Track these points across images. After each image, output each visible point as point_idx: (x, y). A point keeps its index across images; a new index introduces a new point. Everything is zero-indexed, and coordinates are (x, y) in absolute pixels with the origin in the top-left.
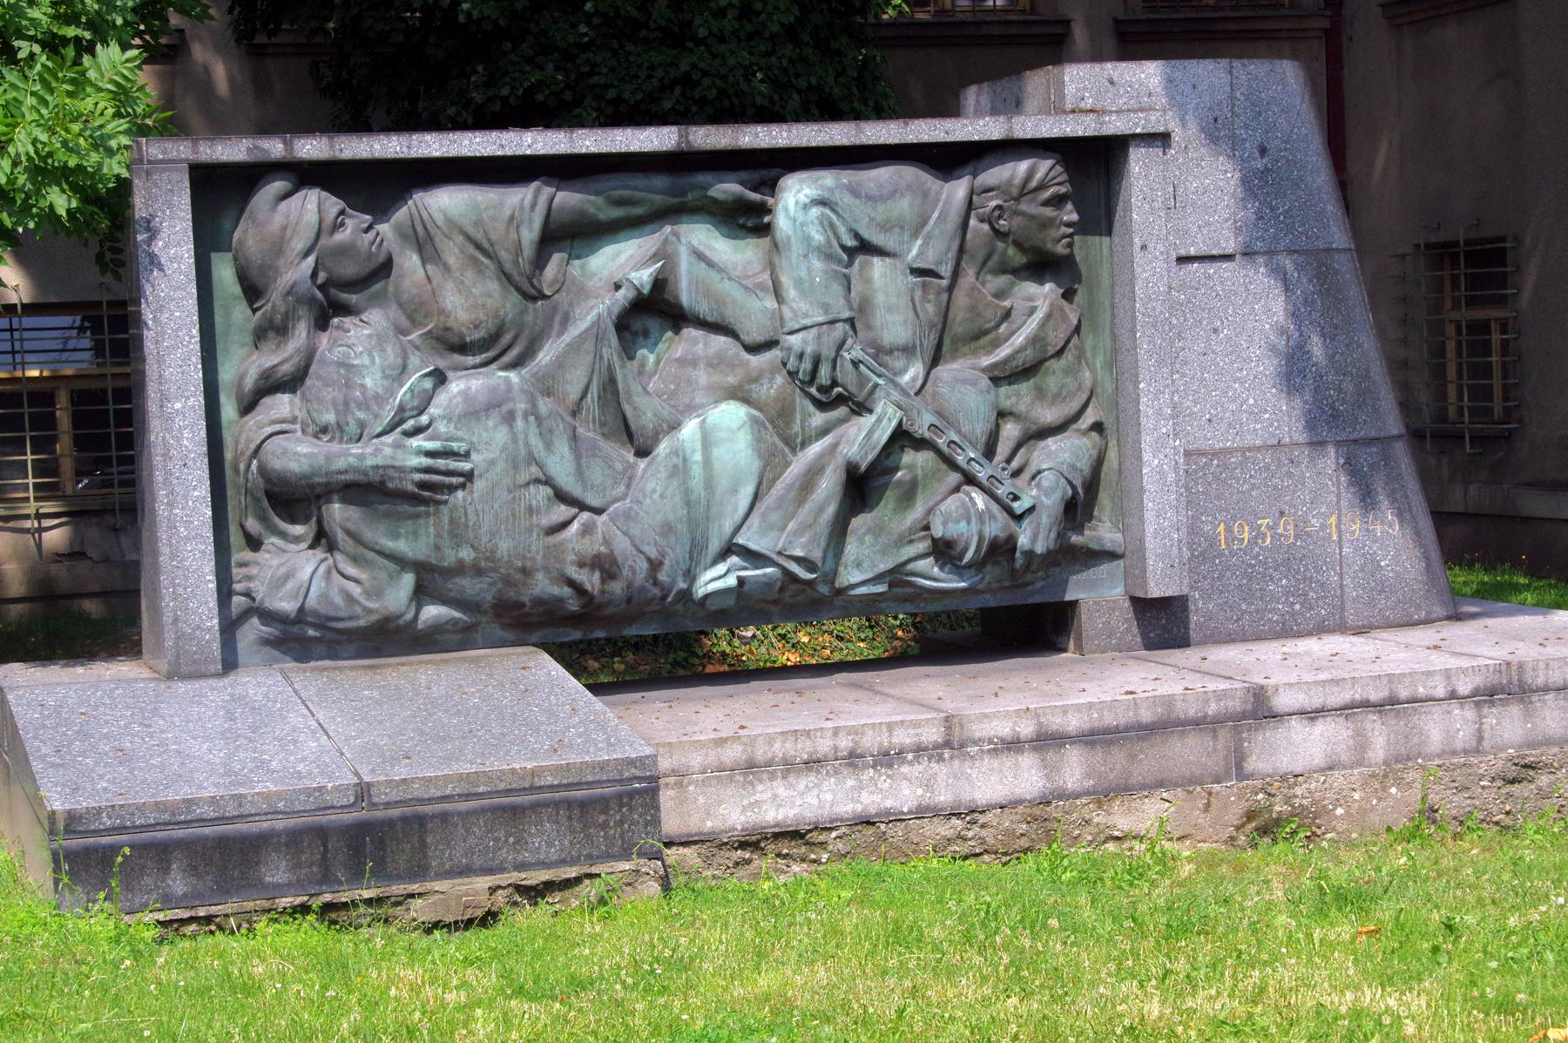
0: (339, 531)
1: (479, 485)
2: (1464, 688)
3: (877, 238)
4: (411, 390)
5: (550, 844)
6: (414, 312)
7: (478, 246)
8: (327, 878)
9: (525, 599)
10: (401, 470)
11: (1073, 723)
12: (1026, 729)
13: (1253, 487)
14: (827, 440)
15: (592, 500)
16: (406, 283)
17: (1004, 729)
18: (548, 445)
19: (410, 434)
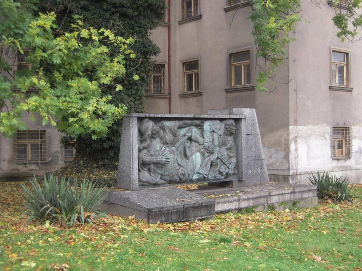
0: (152, 170)
1: (170, 163)
2: (289, 192)
3: (215, 130)
6: (161, 139)
7: (170, 129)
9: (173, 180)
10: (162, 161)
14: (209, 158)
15: (183, 166)
16: (161, 135)
18: (178, 158)
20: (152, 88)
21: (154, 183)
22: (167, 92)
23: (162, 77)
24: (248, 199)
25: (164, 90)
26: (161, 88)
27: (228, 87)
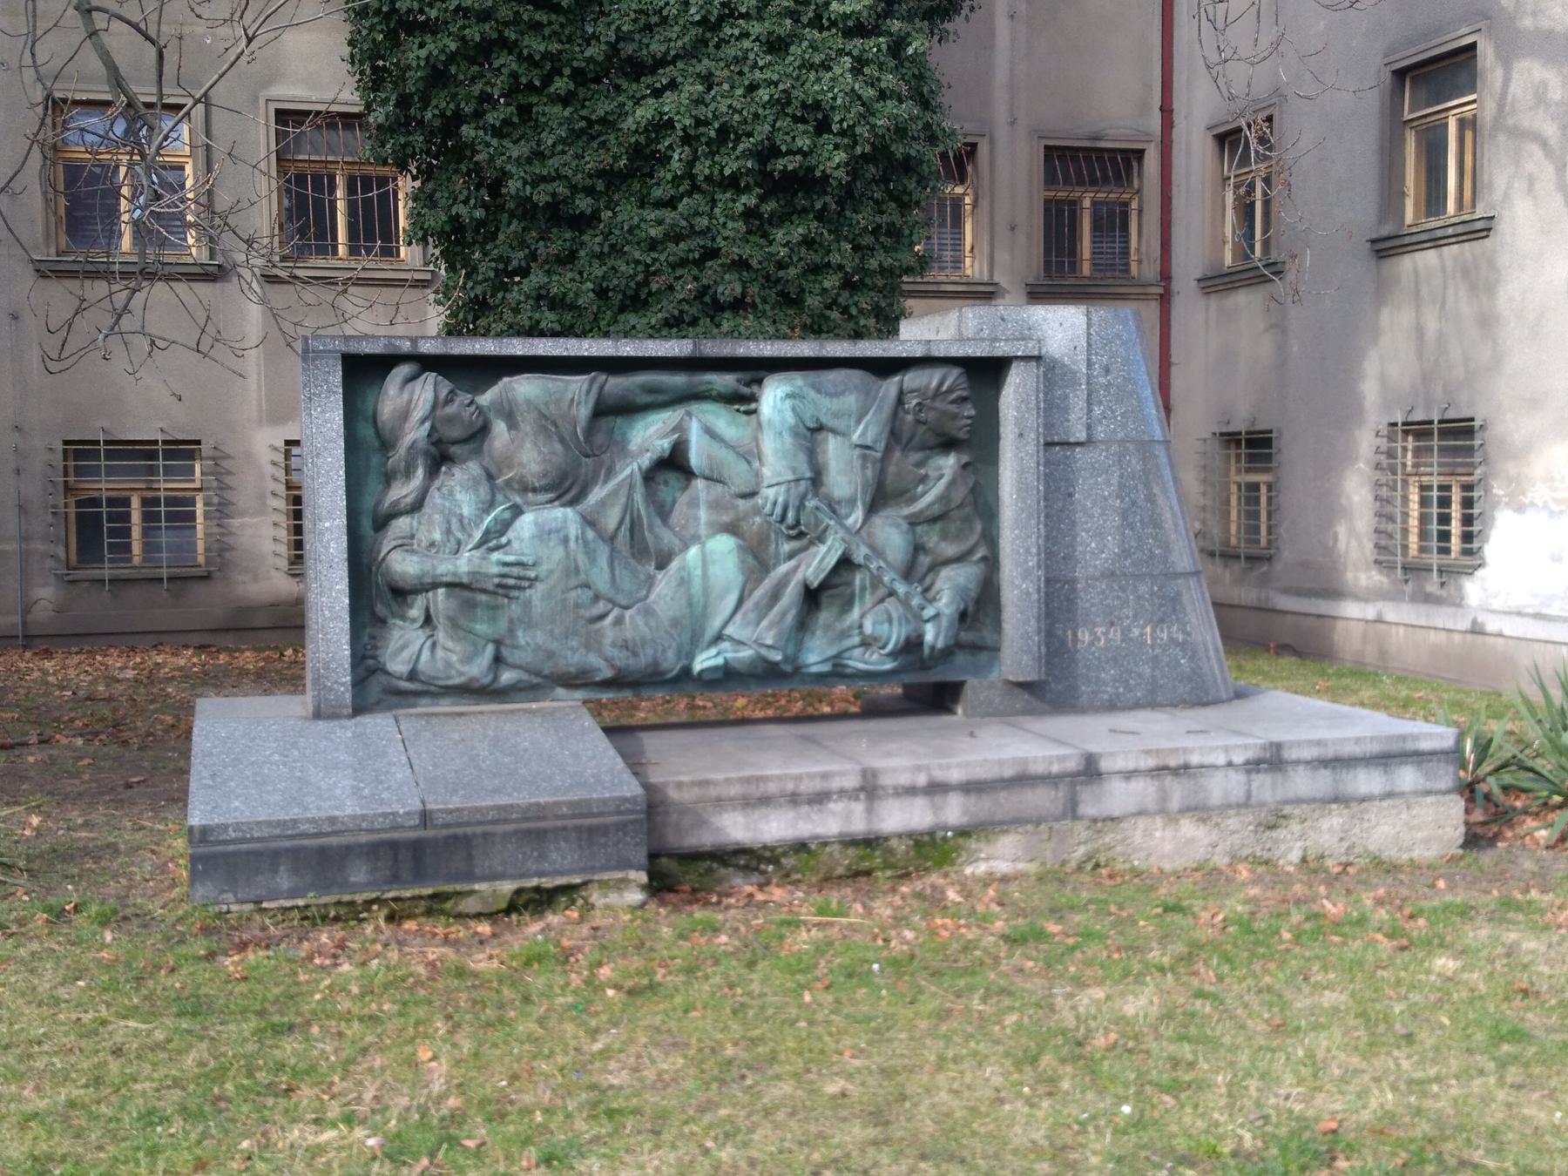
2: (1238, 759)
4: (495, 518)
5: (564, 858)
8: (395, 879)
10: (486, 575)
11: (955, 776)
12: (922, 780)
13: (1093, 605)
14: (793, 563)
17: (904, 779)
19: (492, 550)
20: (1087, 254)
21: (457, 681)
22: (1151, 271)
23: (1134, 205)
24: (936, 789)
25: (1140, 262)
26: (1125, 252)
27: (1386, 231)
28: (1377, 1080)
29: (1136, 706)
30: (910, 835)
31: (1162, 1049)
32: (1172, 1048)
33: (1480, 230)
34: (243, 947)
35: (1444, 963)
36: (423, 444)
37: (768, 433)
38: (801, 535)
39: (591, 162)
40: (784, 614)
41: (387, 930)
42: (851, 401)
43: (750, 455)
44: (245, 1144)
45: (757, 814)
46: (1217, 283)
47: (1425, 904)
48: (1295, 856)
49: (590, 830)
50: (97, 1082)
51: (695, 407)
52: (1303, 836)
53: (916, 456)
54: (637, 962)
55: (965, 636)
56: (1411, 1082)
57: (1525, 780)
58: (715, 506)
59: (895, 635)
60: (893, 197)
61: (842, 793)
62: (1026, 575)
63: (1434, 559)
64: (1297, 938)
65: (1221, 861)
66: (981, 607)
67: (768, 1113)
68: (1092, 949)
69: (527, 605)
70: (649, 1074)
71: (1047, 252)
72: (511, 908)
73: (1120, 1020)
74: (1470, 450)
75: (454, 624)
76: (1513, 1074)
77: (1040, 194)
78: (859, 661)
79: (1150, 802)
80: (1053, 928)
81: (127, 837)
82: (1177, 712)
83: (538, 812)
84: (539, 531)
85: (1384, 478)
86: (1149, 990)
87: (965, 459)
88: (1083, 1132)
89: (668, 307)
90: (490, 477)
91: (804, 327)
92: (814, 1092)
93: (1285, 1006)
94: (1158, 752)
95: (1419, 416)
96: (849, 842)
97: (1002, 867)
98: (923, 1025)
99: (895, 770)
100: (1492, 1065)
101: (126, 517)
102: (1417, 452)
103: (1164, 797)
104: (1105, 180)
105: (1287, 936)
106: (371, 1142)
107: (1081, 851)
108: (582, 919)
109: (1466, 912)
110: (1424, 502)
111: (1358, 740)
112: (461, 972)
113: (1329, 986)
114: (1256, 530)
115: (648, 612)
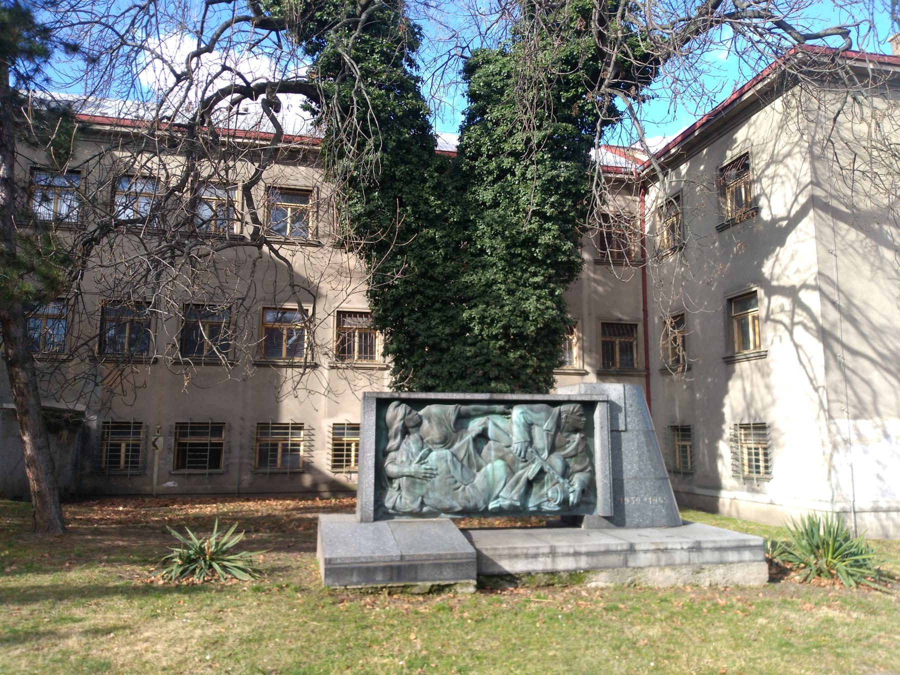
2: (685, 547)
8: (391, 580)
11: (583, 549)
12: (571, 551)
17: (565, 550)
21: (409, 510)
22: (642, 366)
24: (576, 554)
26: (632, 359)
27: (728, 354)
28: (739, 658)
29: (647, 527)
30: (568, 571)
31: (663, 645)
32: (667, 646)
33: (762, 356)
34: (342, 601)
35: (762, 621)
36: (400, 428)
37: (512, 425)
38: (526, 461)
39: (447, 330)
40: (520, 489)
41: (388, 599)
42: (543, 415)
43: (508, 433)
44: (361, 662)
45: (514, 561)
46: (664, 372)
47: (756, 602)
48: (707, 584)
49: (456, 564)
50: (309, 640)
51: (490, 416)
52: (709, 577)
53: (565, 434)
54: (476, 611)
55: (584, 499)
56: (750, 659)
57: (791, 558)
58: (497, 450)
59: (560, 498)
60: (551, 342)
61: (543, 554)
62: (605, 477)
63: (754, 475)
64: (709, 611)
65: (680, 584)
66: (589, 489)
67: (530, 660)
68: (636, 613)
69: (433, 483)
70: (488, 647)
71: (603, 360)
72: (430, 591)
73: (648, 636)
74: (765, 435)
75: (408, 490)
76: (787, 657)
77: (600, 339)
78: (546, 507)
79: (654, 563)
80: (622, 606)
81: (294, 564)
82: (662, 529)
83: (439, 557)
84: (438, 457)
85: (733, 444)
86: (658, 626)
87: (582, 435)
88: (638, 670)
89: (473, 379)
90: (422, 439)
91: (520, 386)
92: (544, 655)
93: (705, 633)
94: (656, 543)
95: (746, 421)
96: (546, 573)
97: (601, 584)
98: (579, 636)
99: (562, 546)
100: (779, 654)
101: (276, 450)
102: (745, 435)
103: (659, 560)
104: (624, 334)
105: (705, 610)
106: (401, 663)
107: (630, 579)
108: (454, 597)
109: (769, 604)
110: (750, 454)
111: (728, 541)
112: (417, 613)
113: (721, 627)
114: (686, 463)
115: (474, 487)
